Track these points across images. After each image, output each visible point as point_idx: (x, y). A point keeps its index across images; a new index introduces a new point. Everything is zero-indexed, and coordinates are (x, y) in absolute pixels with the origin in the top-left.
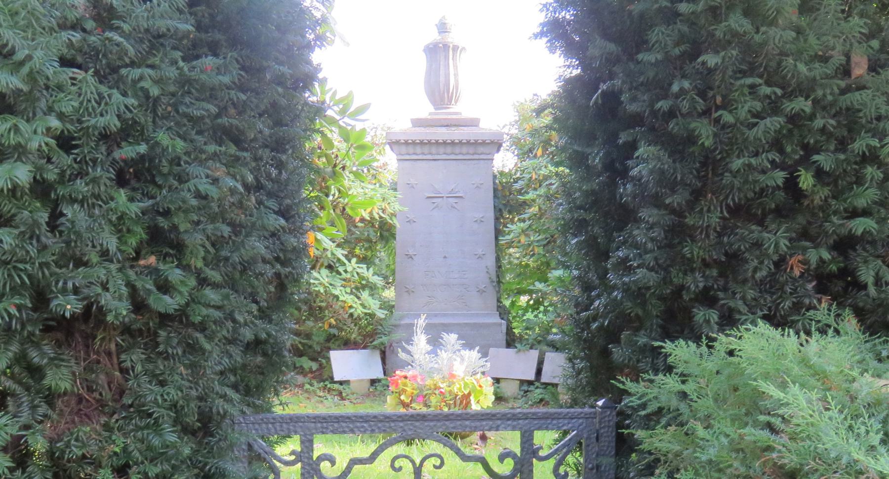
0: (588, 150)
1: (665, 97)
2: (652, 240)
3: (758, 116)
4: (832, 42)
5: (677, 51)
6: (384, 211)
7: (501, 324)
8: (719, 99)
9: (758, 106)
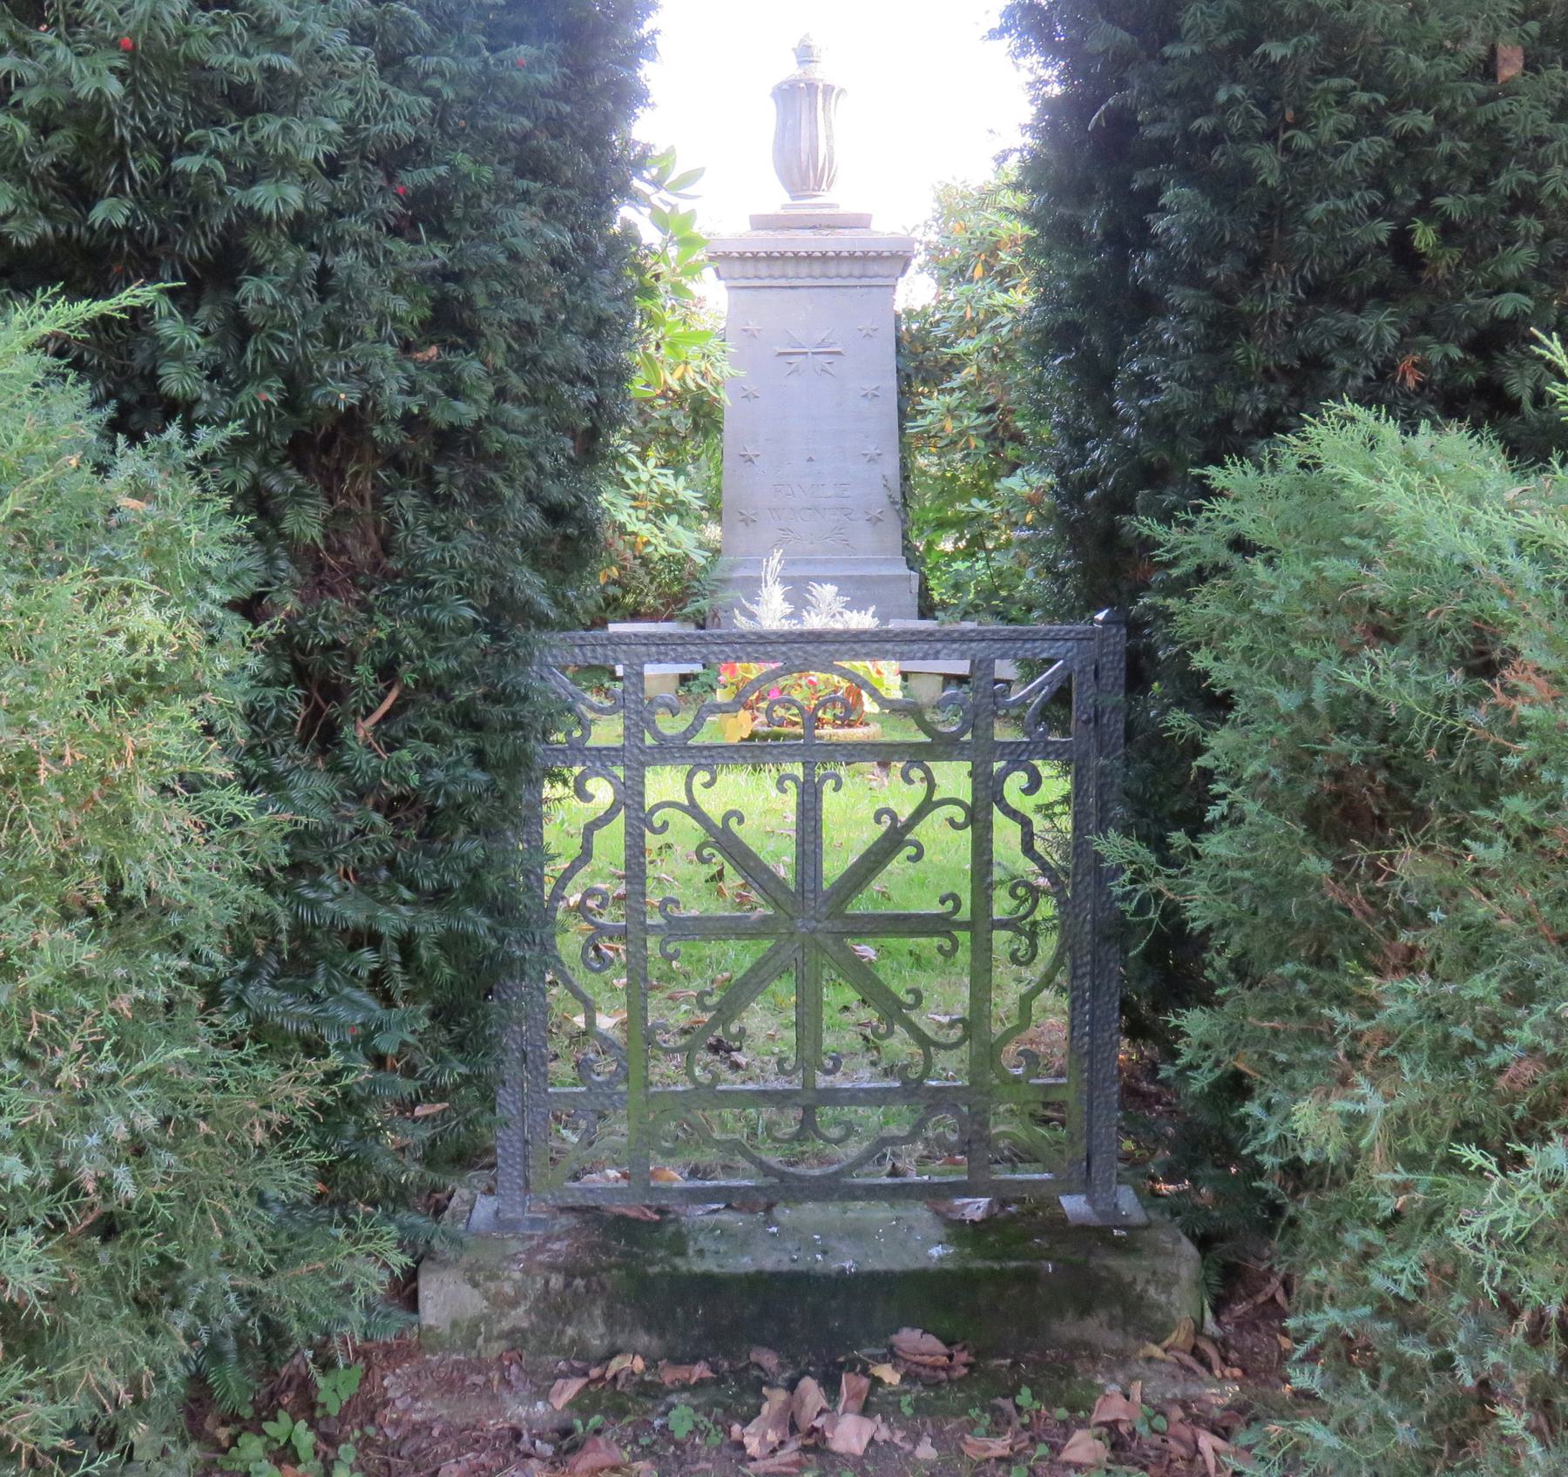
0: (1081, 213)
1: (1207, 112)
2: (1187, 338)
3: (1352, 136)
4: (1465, 23)
5: (1225, 40)
6: (704, 375)
7: (909, 578)
8: (1289, 115)
9: (1349, 120)
